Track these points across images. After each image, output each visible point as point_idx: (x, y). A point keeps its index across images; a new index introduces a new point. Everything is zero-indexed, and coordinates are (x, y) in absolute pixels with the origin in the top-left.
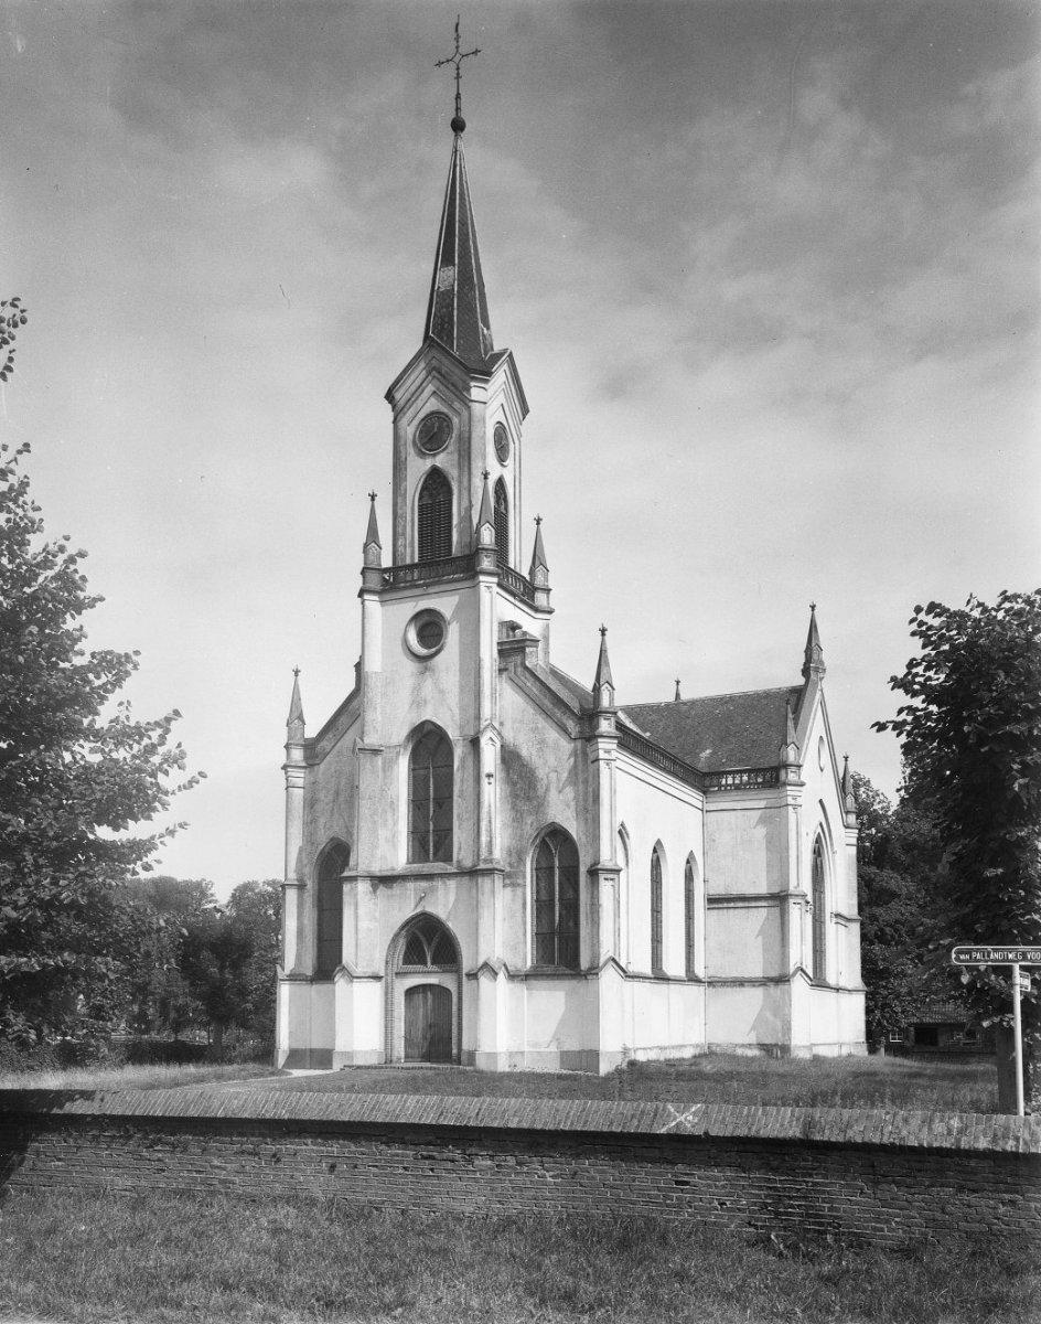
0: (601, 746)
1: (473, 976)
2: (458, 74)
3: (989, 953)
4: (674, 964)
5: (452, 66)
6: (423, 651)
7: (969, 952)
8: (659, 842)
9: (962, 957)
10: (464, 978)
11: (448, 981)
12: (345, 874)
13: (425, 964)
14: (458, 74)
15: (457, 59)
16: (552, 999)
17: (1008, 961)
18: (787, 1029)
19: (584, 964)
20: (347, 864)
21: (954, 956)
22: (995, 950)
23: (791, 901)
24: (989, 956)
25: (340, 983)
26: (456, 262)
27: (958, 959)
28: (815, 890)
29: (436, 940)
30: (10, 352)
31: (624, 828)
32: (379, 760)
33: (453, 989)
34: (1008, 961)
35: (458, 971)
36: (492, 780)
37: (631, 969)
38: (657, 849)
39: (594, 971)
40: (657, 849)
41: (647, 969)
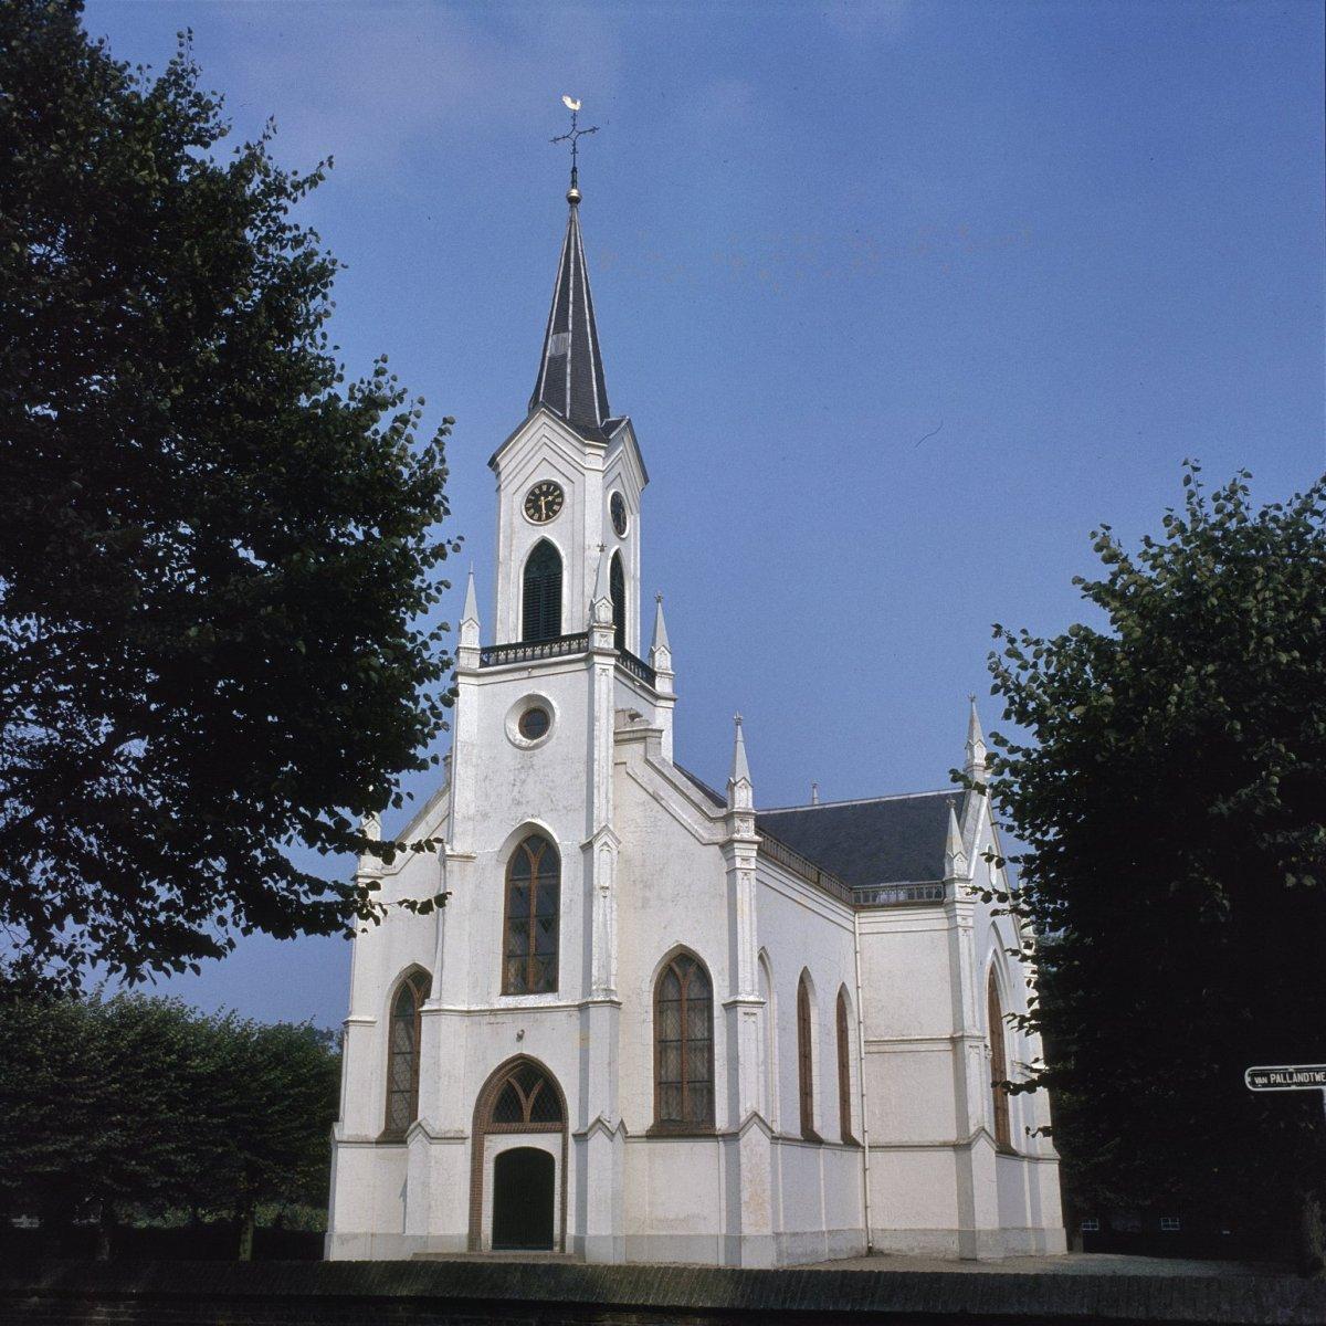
0: (737, 852)
1: (581, 1138)
2: (574, 149)
3: (1291, 1074)
4: (826, 1123)
5: (569, 142)
6: (525, 742)
7: (1265, 1074)
8: (806, 967)
9: (1258, 1080)
10: (571, 1140)
11: (546, 1142)
12: (425, 1008)
13: (520, 1119)
14: (574, 149)
15: (573, 136)
16: (694, 1160)
17: (1316, 1083)
18: (951, 1231)
19: (722, 1122)
20: (428, 996)
21: (1248, 1080)
22: (1298, 1071)
23: (967, 1044)
24: (1291, 1078)
25: (416, 1143)
26: (570, 327)
27: (1253, 1083)
28: (992, 1032)
29: (535, 1091)
30: (445, 421)
31: (765, 952)
32: (470, 867)
33: (557, 1157)
34: (1316, 1083)
35: (564, 1130)
36: (608, 893)
37: (777, 1128)
38: (804, 981)
39: (732, 1137)
40: (804, 981)
41: (796, 1131)
